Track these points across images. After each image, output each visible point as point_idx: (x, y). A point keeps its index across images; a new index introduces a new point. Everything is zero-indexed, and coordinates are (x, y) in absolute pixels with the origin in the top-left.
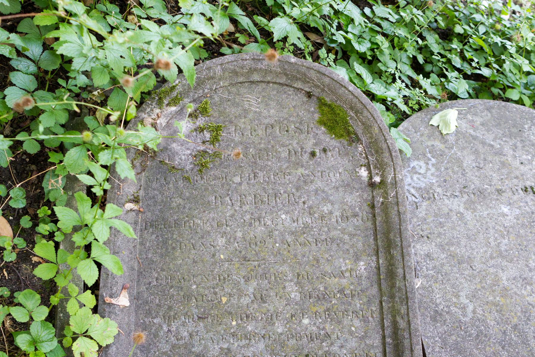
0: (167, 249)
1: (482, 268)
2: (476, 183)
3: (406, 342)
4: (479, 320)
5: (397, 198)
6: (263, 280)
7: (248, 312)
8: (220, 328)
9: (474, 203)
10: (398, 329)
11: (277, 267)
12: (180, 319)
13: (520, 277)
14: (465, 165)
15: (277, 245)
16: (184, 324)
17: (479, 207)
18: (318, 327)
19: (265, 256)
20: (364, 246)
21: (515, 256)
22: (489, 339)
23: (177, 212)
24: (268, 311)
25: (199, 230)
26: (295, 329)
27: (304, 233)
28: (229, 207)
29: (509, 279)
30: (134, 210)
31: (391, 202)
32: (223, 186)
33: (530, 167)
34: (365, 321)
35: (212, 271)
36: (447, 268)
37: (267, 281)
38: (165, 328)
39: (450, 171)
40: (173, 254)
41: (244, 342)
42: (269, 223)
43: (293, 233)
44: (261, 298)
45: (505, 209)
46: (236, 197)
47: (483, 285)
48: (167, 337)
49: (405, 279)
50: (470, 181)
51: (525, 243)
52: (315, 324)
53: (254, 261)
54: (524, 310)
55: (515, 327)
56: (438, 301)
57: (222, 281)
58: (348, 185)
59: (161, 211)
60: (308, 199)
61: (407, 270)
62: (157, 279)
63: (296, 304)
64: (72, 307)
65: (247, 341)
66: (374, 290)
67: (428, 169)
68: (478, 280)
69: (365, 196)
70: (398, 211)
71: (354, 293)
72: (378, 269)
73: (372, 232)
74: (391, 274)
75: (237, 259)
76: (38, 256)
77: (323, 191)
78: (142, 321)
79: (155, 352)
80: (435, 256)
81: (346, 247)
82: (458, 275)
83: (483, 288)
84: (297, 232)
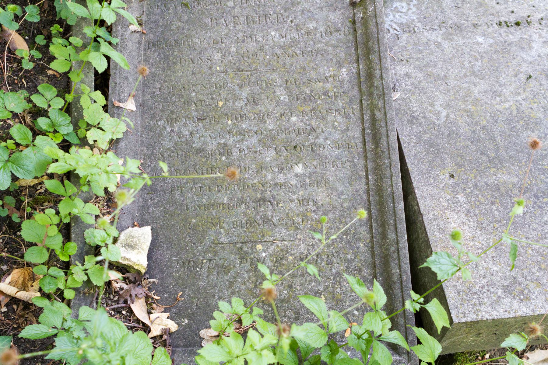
0: (168, 64)
1: (456, 84)
2: (453, 18)
3: (383, 130)
4: (451, 123)
5: (375, 11)
6: (255, 86)
7: (243, 113)
8: (217, 127)
9: (451, 34)
10: (376, 120)
11: (268, 75)
12: (181, 121)
13: (491, 90)
14: (444, 5)
15: (268, 57)
16: (185, 125)
17: (456, 38)
18: (305, 124)
19: (257, 66)
20: (346, 55)
21: (487, 75)
22: (460, 137)
23: (177, 33)
24: (260, 111)
25: (197, 47)
26: (285, 126)
27: (292, 46)
28: (223, 27)
29: (480, 92)
30: (137, 32)
31: (370, 16)
32: (218, 10)
33: (506, 6)
34: (346, 117)
35: (209, 81)
36: (424, 84)
37: (258, 87)
38: (168, 129)
39: (430, 10)
40: (174, 68)
41: (239, 137)
42: (260, 39)
43: (281, 47)
44: (254, 101)
45: (480, 39)
46: (230, 19)
47: (456, 97)
48: (170, 136)
49: (382, 79)
50: (449, 18)
51: (497, 65)
52: (302, 121)
53: (247, 71)
54: (492, 115)
55: (484, 128)
56: (415, 109)
57: (219, 88)
58: (331, 5)
59: (162, 33)
60: (295, 18)
61: (383, 70)
62: (160, 89)
63: (285, 105)
64: (85, 102)
65: (242, 137)
66: (355, 92)
67: (409, 9)
68: (452, 93)
69: (347, 14)
70: (377, 23)
71: (337, 94)
72: (359, 74)
73: (353, 44)
74: (370, 76)
75: (232, 70)
76: (52, 70)
77: (309, 11)
78: (147, 124)
79: (160, 149)
80: (413, 75)
81: (330, 57)
82: (433, 90)
83: (456, 99)
84: (285, 46)
